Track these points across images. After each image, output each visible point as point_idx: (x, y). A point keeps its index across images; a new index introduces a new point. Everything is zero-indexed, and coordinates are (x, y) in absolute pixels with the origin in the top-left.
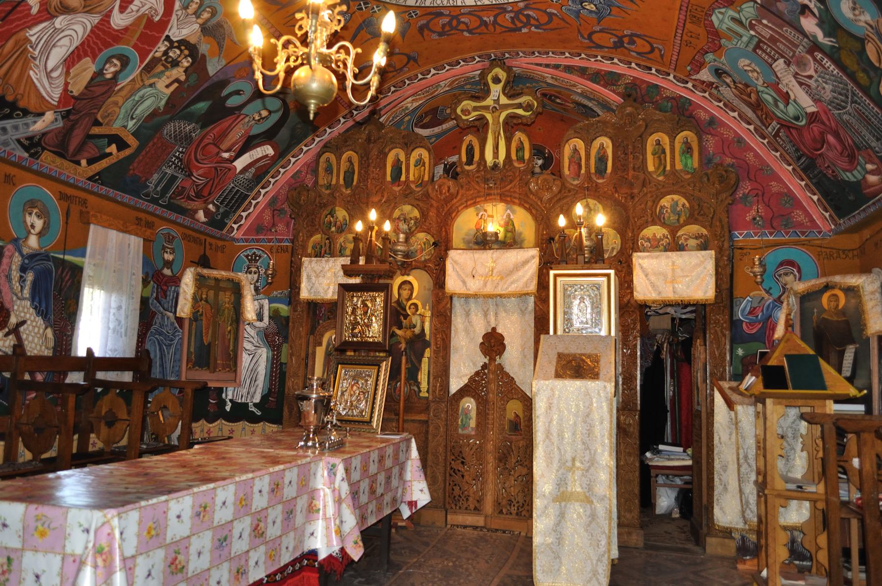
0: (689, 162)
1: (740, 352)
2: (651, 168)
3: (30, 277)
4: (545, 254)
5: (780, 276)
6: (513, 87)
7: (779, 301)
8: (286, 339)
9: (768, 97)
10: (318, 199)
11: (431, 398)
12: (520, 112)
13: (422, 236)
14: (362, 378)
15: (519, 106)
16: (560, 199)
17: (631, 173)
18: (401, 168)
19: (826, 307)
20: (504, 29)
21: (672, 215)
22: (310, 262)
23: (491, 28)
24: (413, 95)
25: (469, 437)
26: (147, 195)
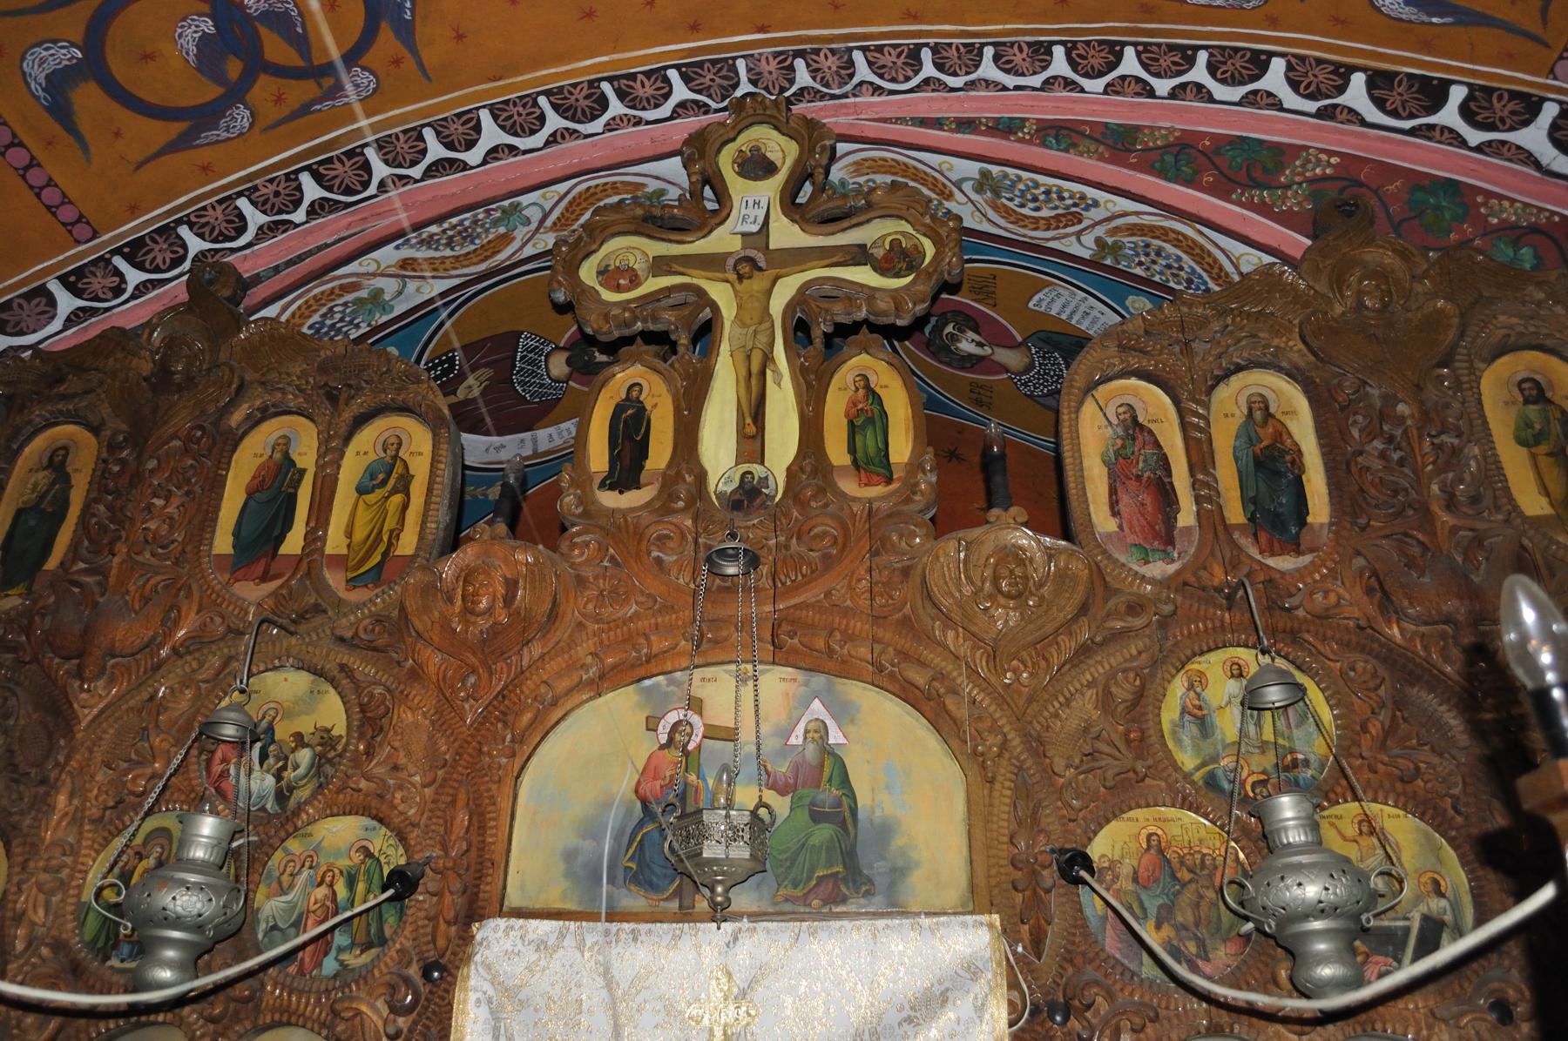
4: (1037, 943)
12: (863, 275)
16: (1085, 651)
18: (291, 501)
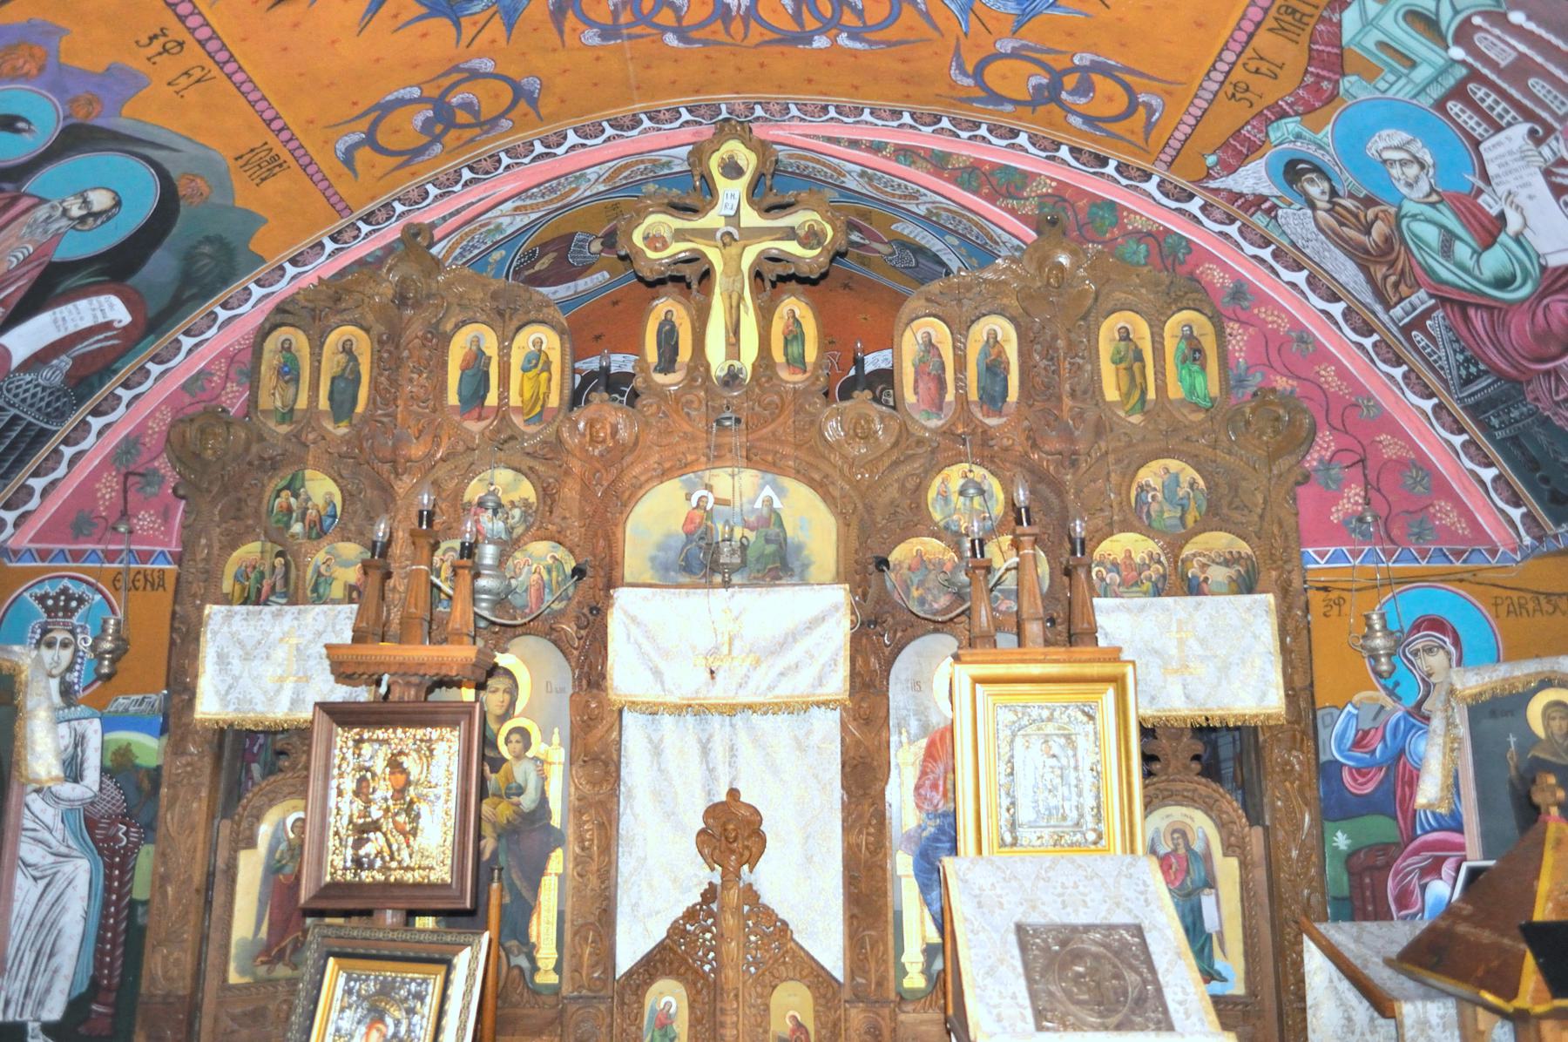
0: (1199, 380)
1: (1341, 841)
2: (1111, 394)
4: (864, 596)
6: (774, 189)
7: (1419, 715)
8: (149, 830)
10: (255, 448)
11: (566, 990)
12: (792, 247)
13: (541, 552)
15: (790, 234)
16: (896, 464)
17: (1067, 402)
19: (1540, 731)
20: (769, 36)
21: (1166, 507)
22: (229, 617)
23: (737, 27)
24: (518, 195)
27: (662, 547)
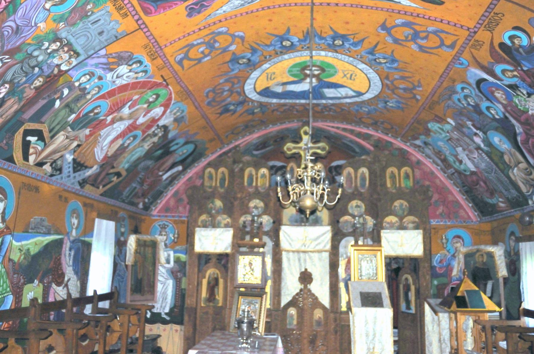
1: (436, 282)
3: (73, 253)
5: (454, 243)
6: (316, 137)
7: (454, 256)
8: (185, 275)
9: (451, 159)
14: (253, 304)
25: (293, 330)
26: (121, 199)
27: (291, 217)
